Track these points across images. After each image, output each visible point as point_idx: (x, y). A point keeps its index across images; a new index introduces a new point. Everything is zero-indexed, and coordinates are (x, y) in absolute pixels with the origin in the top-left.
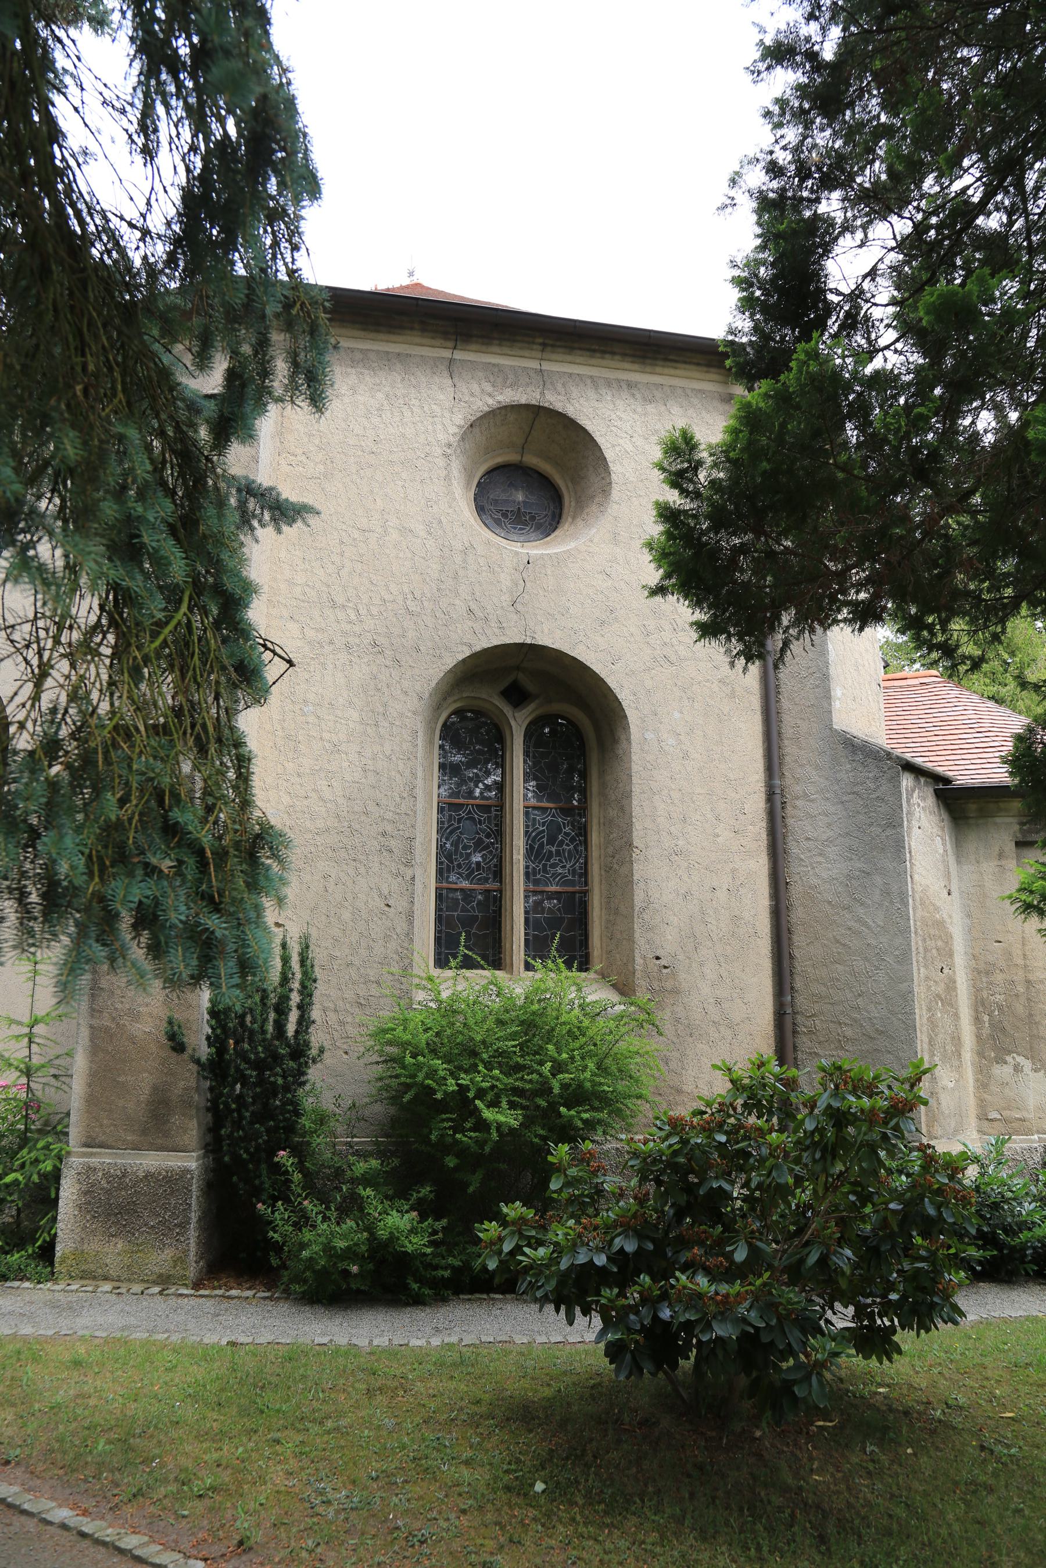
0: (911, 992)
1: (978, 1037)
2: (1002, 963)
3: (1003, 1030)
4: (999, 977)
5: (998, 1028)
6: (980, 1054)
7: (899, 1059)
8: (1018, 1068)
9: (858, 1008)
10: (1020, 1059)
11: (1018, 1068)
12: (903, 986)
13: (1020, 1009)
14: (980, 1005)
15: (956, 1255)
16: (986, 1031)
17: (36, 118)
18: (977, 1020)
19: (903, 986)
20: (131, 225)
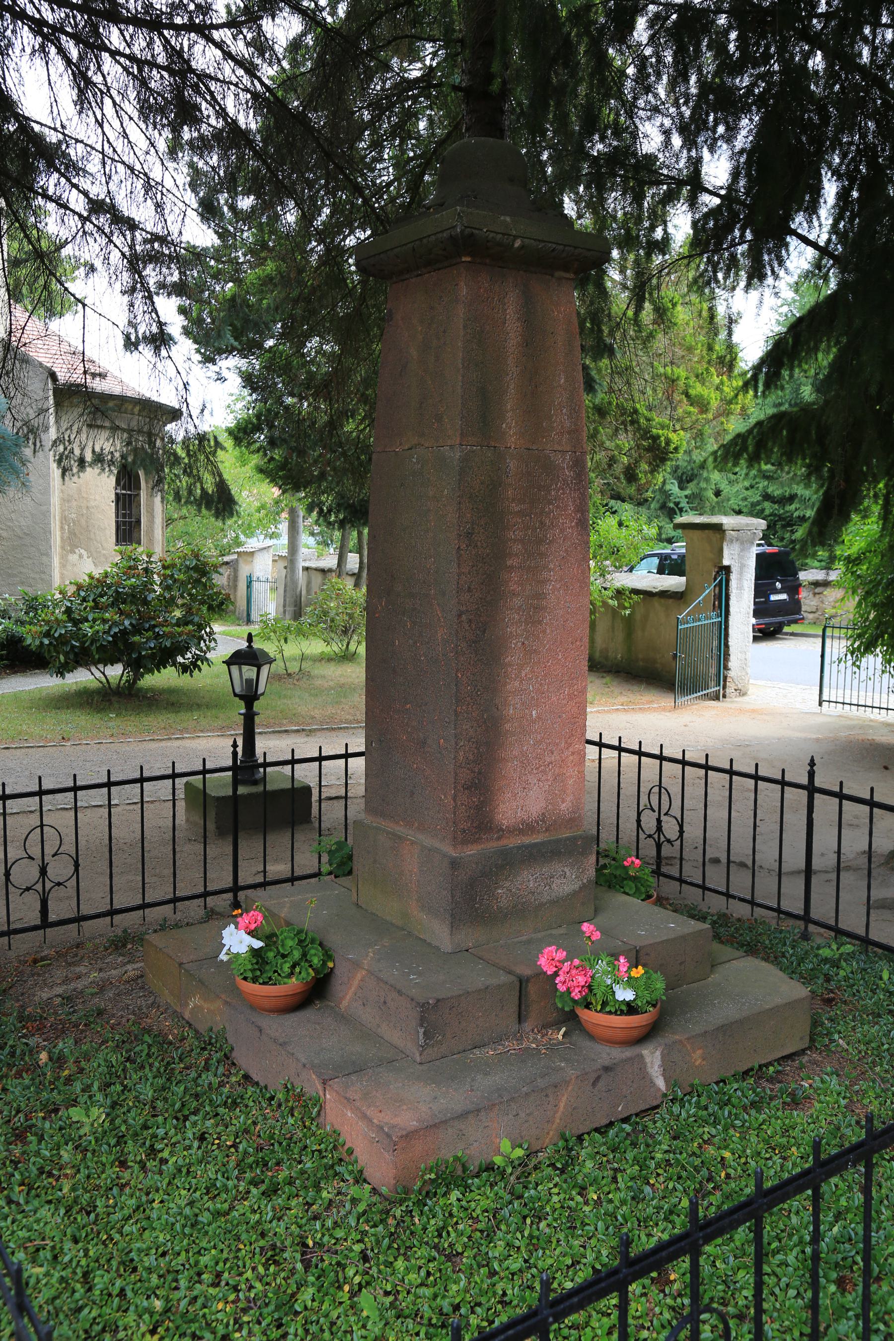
0: (49, 511)
1: (62, 538)
2: (76, 496)
3: (75, 534)
4: (74, 504)
5: (72, 533)
6: (63, 548)
7: (39, 550)
8: (81, 556)
9: (11, 520)
10: (82, 551)
11: (81, 556)
12: (44, 508)
13: (83, 522)
14: (64, 519)
15: (883, 637)
16: (66, 535)
17: (785, 433)
18: (62, 528)
19: (44, 508)
20: (50, 128)
